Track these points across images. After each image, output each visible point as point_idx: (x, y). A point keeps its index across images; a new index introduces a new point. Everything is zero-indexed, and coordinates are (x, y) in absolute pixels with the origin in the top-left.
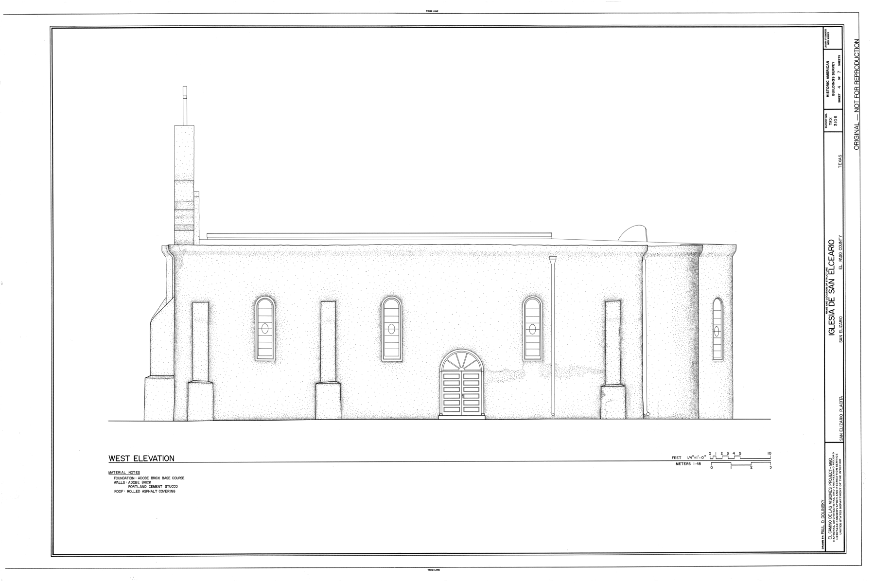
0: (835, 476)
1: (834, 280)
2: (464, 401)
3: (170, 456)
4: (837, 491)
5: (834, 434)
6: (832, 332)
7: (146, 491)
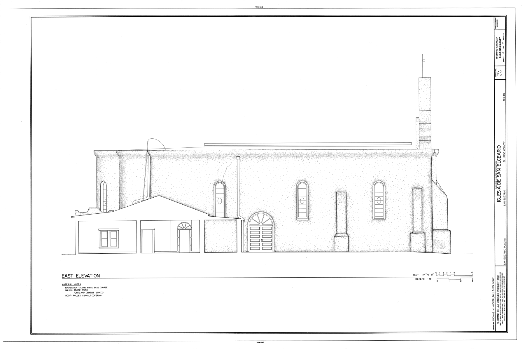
0: (501, 286)
1: (500, 169)
2: (262, 243)
3: (97, 274)
4: (502, 295)
5: (500, 261)
6: (499, 200)
7: (85, 296)
